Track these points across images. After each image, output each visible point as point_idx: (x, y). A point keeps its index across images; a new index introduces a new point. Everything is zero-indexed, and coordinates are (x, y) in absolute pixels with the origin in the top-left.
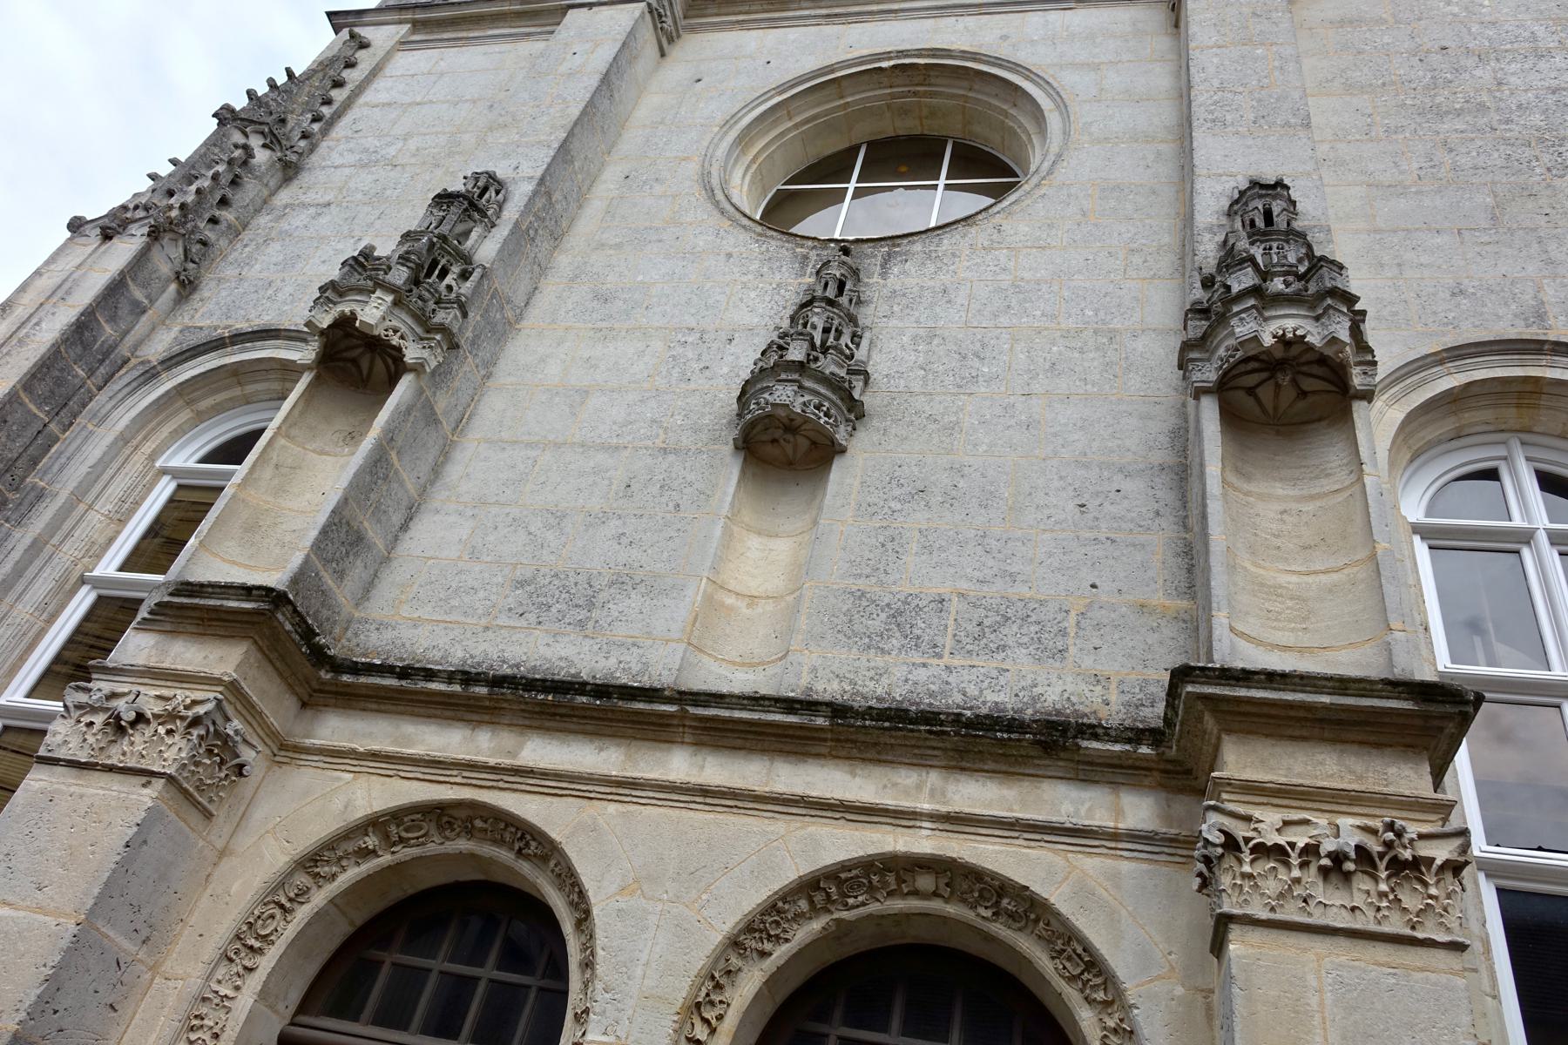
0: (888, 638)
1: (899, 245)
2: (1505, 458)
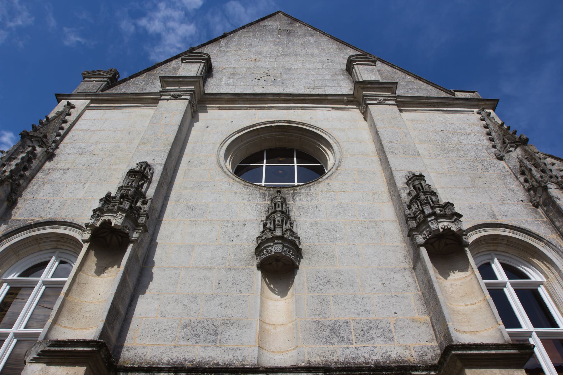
1: (296, 190)
2: (491, 259)
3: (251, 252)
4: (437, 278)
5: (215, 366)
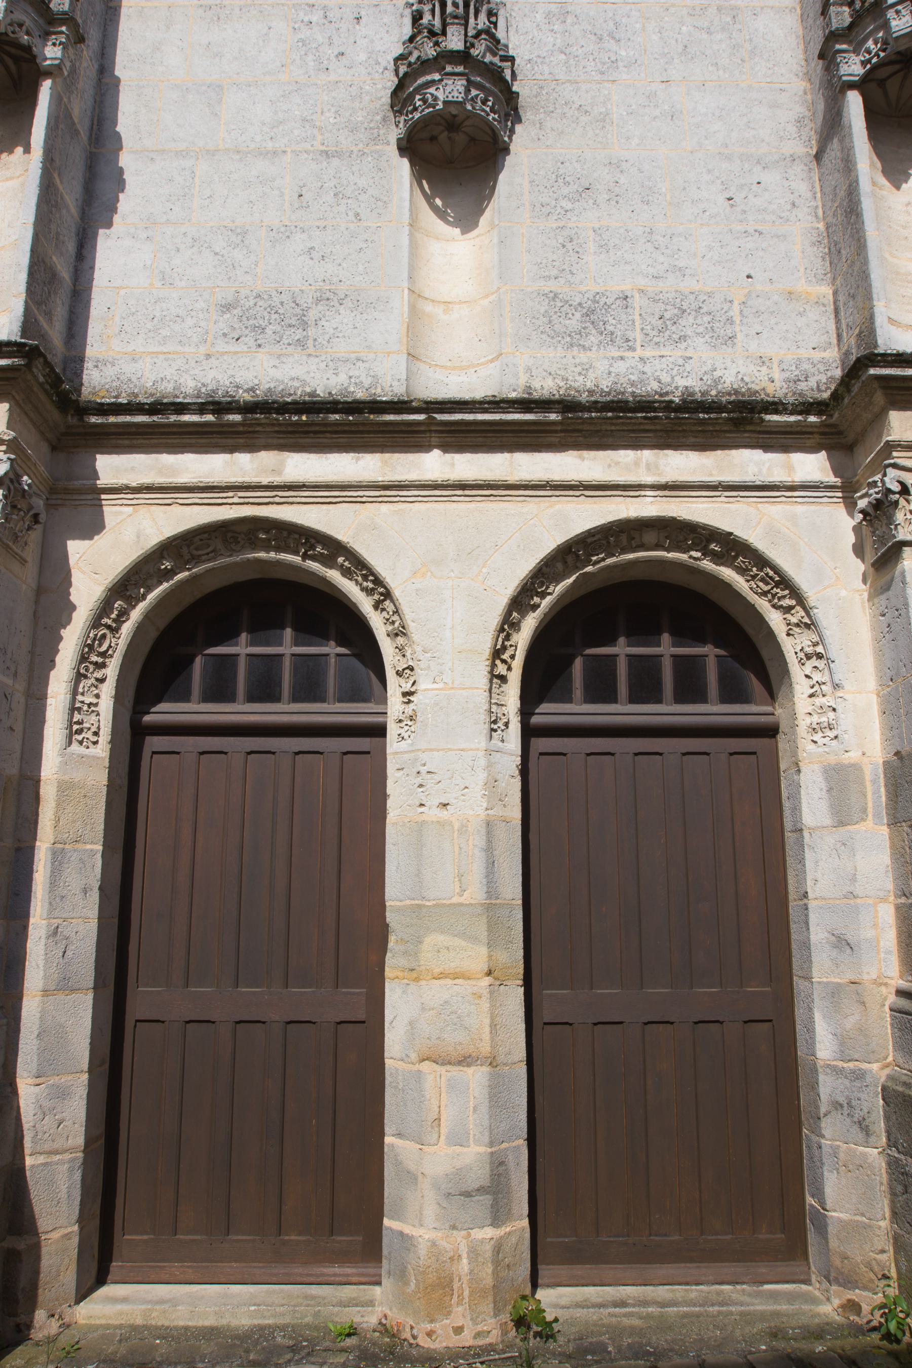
0: (587, 336)
3: (380, 103)
4: (874, 184)
5: (307, 398)
